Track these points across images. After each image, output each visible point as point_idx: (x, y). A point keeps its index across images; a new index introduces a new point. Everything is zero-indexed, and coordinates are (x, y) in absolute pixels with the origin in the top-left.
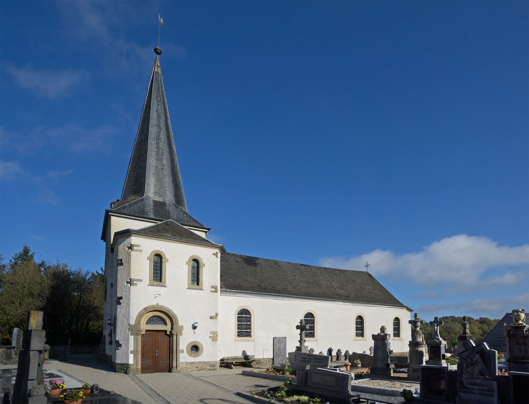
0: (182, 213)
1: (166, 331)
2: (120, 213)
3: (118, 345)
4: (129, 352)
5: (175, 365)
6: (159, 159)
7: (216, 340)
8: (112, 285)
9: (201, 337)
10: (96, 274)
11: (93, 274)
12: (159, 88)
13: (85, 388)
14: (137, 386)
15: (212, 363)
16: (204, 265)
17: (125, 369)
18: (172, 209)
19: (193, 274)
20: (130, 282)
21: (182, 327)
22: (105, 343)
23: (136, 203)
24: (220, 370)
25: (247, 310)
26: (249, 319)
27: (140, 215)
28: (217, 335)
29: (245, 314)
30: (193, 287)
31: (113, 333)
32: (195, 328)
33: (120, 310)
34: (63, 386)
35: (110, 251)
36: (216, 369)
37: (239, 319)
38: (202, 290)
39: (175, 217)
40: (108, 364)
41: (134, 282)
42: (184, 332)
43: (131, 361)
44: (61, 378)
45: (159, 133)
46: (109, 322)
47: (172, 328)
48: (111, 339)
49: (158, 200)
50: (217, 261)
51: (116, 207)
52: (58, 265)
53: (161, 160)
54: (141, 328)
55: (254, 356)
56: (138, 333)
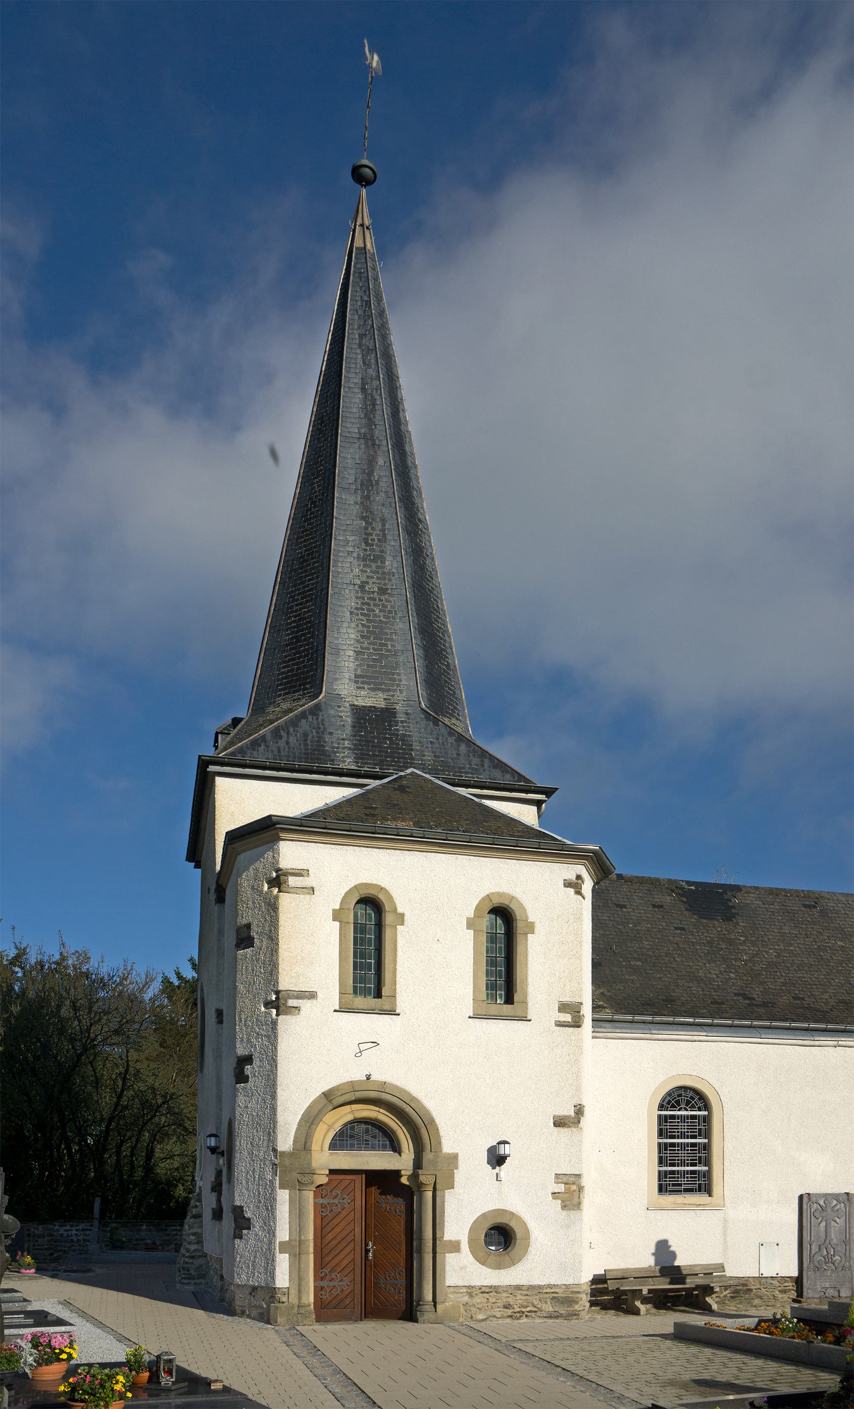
0: (451, 740)
1: (397, 1174)
2: (245, 765)
3: (242, 1223)
4: (284, 1245)
5: (428, 1296)
6: (372, 557)
7: (578, 1206)
8: (219, 1013)
9: (519, 1191)
10: (176, 982)
11: (166, 981)
12: (368, 303)
13: (132, 1365)
14: (298, 1365)
15: (561, 1293)
16: (531, 928)
17: (263, 1305)
18: (416, 732)
19: (491, 962)
20: (279, 1003)
21: (455, 1157)
22: (199, 1216)
23: (294, 723)
24: (592, 1320)
25: (680, 1088)
26: (704, 1127)
27: (308, 766)
28: (581, 1189)
29: (689, 1105)
30: (494, 1009)
31: (224, 1179)
32: (497, 1159)
33: (245, 1103)
34: (70, 1355)
35: (213, 897)
36: (575, 1315)
37: (665, 1127)
38: (524, 1019)
39: (429, 757)
40: (210, 1292)
41: (292, 1003)
42: (459, 1176)
43: (282, 1279)
44: (68, 1328)
45: (371, 462)
46: (212, 1142)
47: (418, 1163)
48: (219, 1201)
49: (369, 703)
50: (583, 908)
51: (232, 743)
52: (63, 958)
53: (380, 558)
54: (314, 1164)
55: (721, 1267)
56: (304, 1179)
